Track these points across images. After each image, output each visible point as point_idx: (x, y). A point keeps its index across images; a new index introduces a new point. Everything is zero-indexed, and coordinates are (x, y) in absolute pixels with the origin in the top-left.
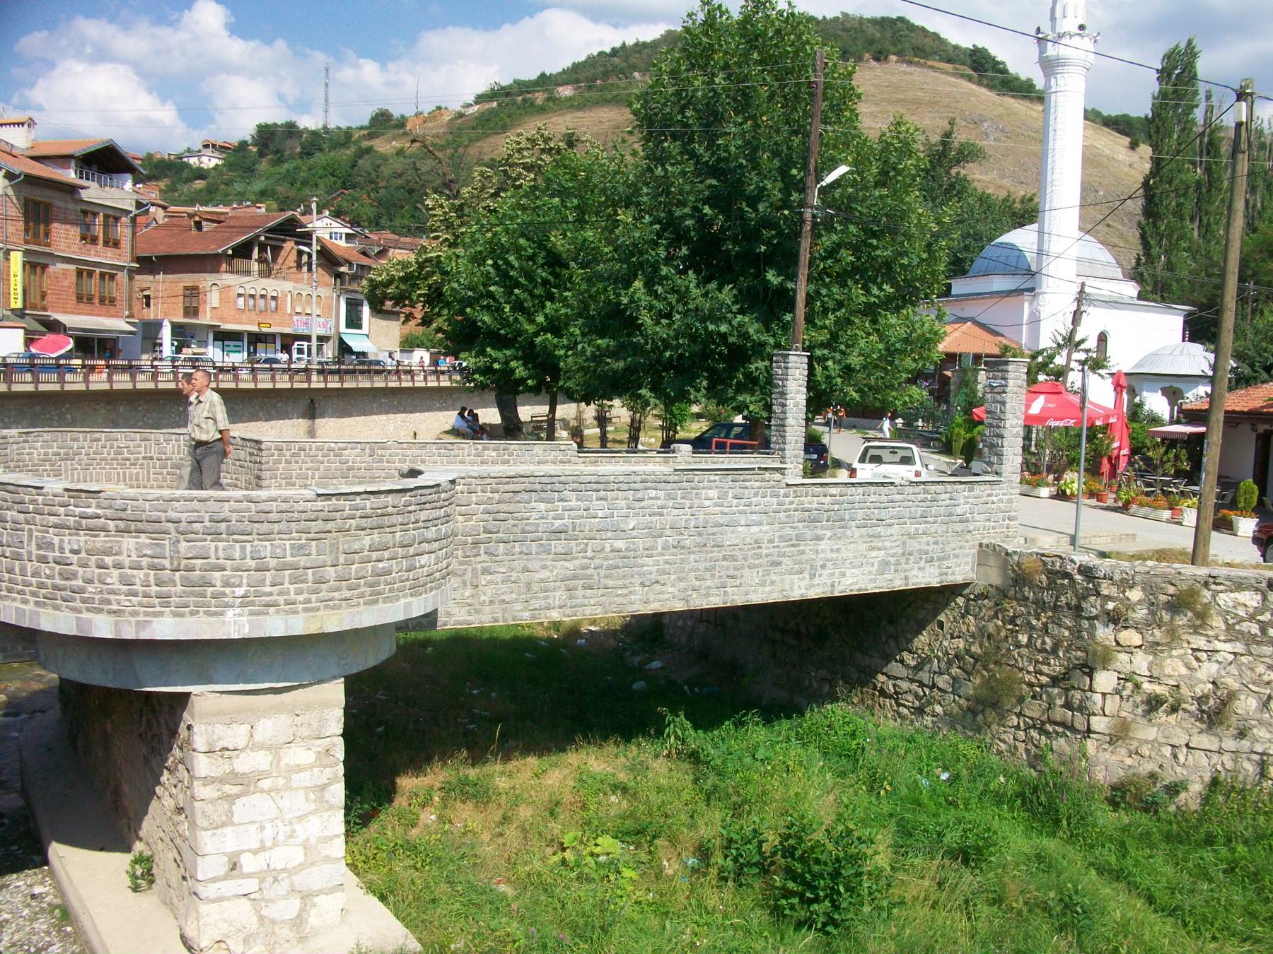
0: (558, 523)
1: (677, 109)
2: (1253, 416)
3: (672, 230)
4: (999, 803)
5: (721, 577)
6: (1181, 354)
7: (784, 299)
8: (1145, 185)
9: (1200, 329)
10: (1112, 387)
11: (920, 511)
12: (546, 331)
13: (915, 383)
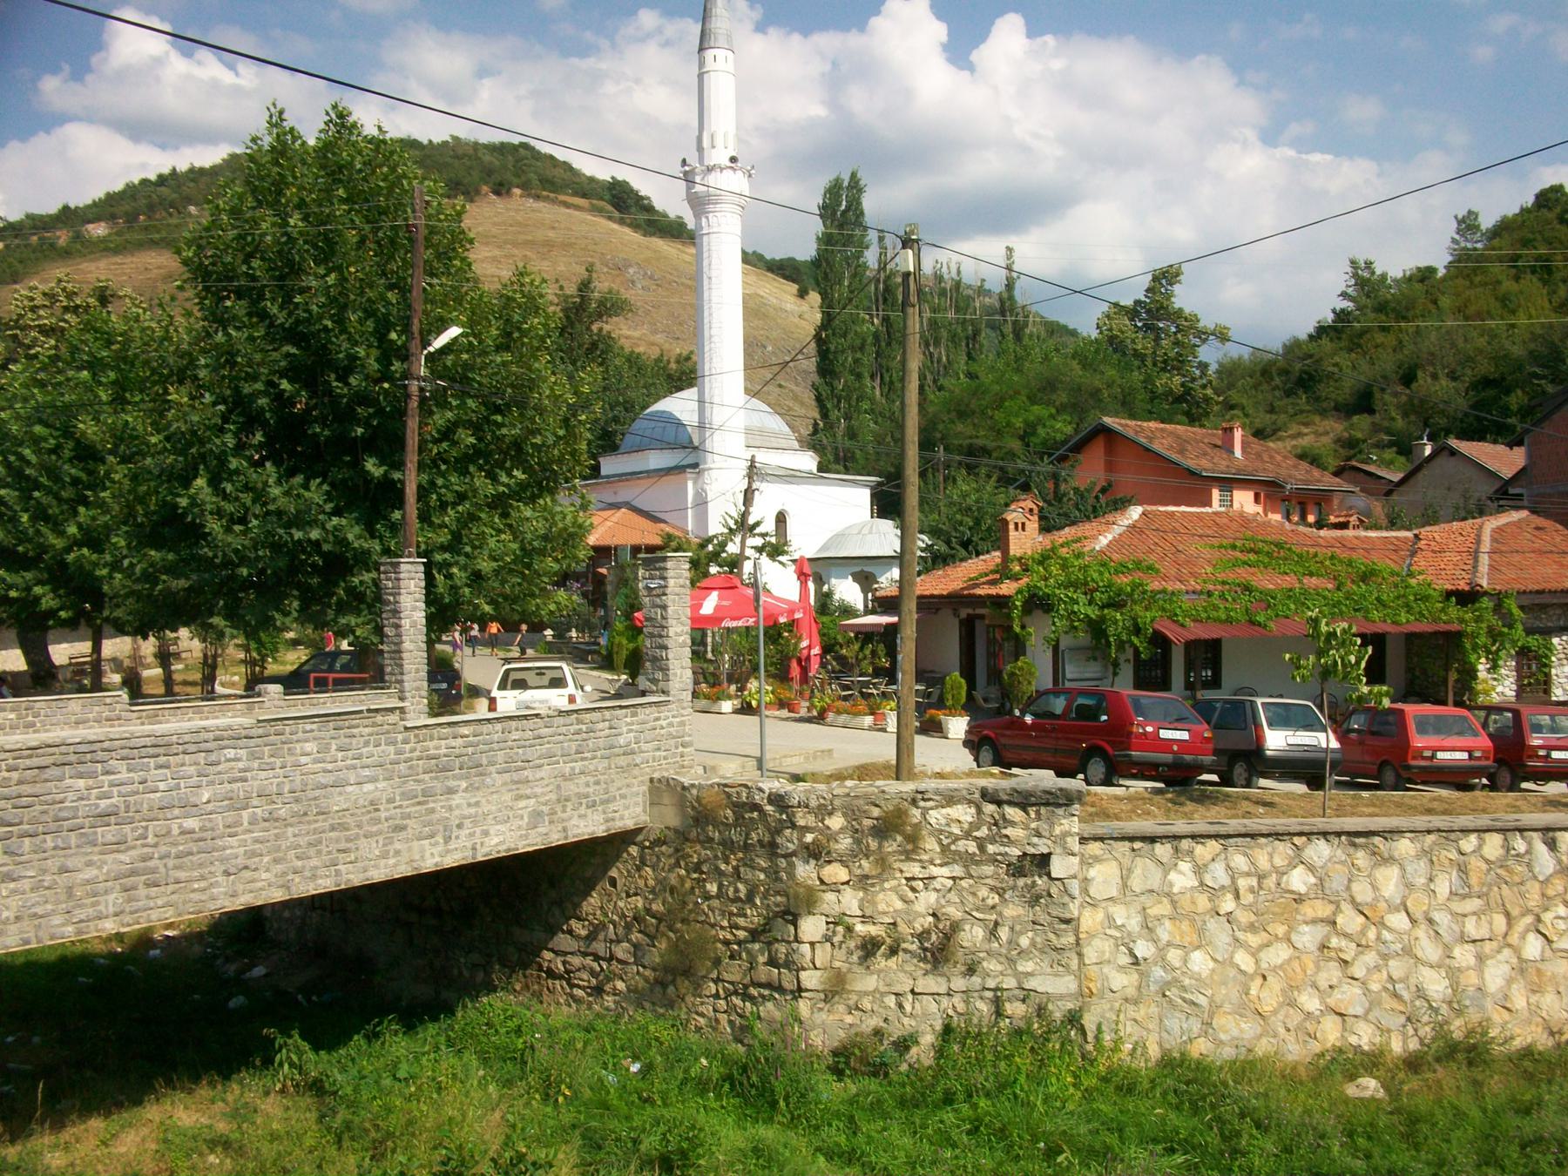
0: (103, 803)
1: (241, 257)
2: (954, 600)
3: (241, 410)
4: (703, 1092)
5: (329, 853)
7: (391, 494)
8: (818, 338)
9: (887, 505)
10: (795, 576)
11: (574, 746)
12: (80, 545)
13: (564, 585)
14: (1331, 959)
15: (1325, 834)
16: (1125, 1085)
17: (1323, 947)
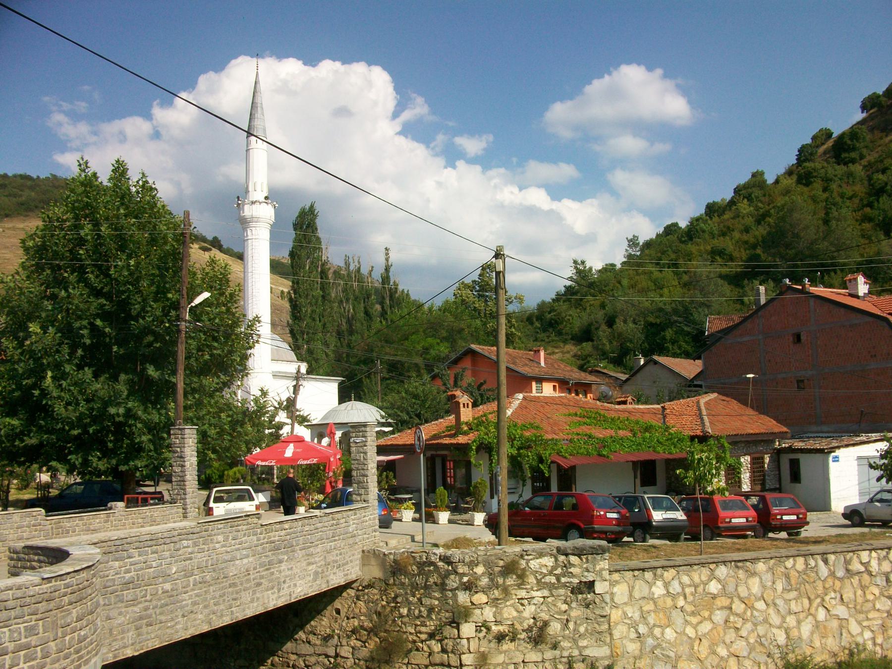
0: (128, 576)
7: (169, 389)
14: (730, 628)
15: (724, 562)
17: (726, 621)
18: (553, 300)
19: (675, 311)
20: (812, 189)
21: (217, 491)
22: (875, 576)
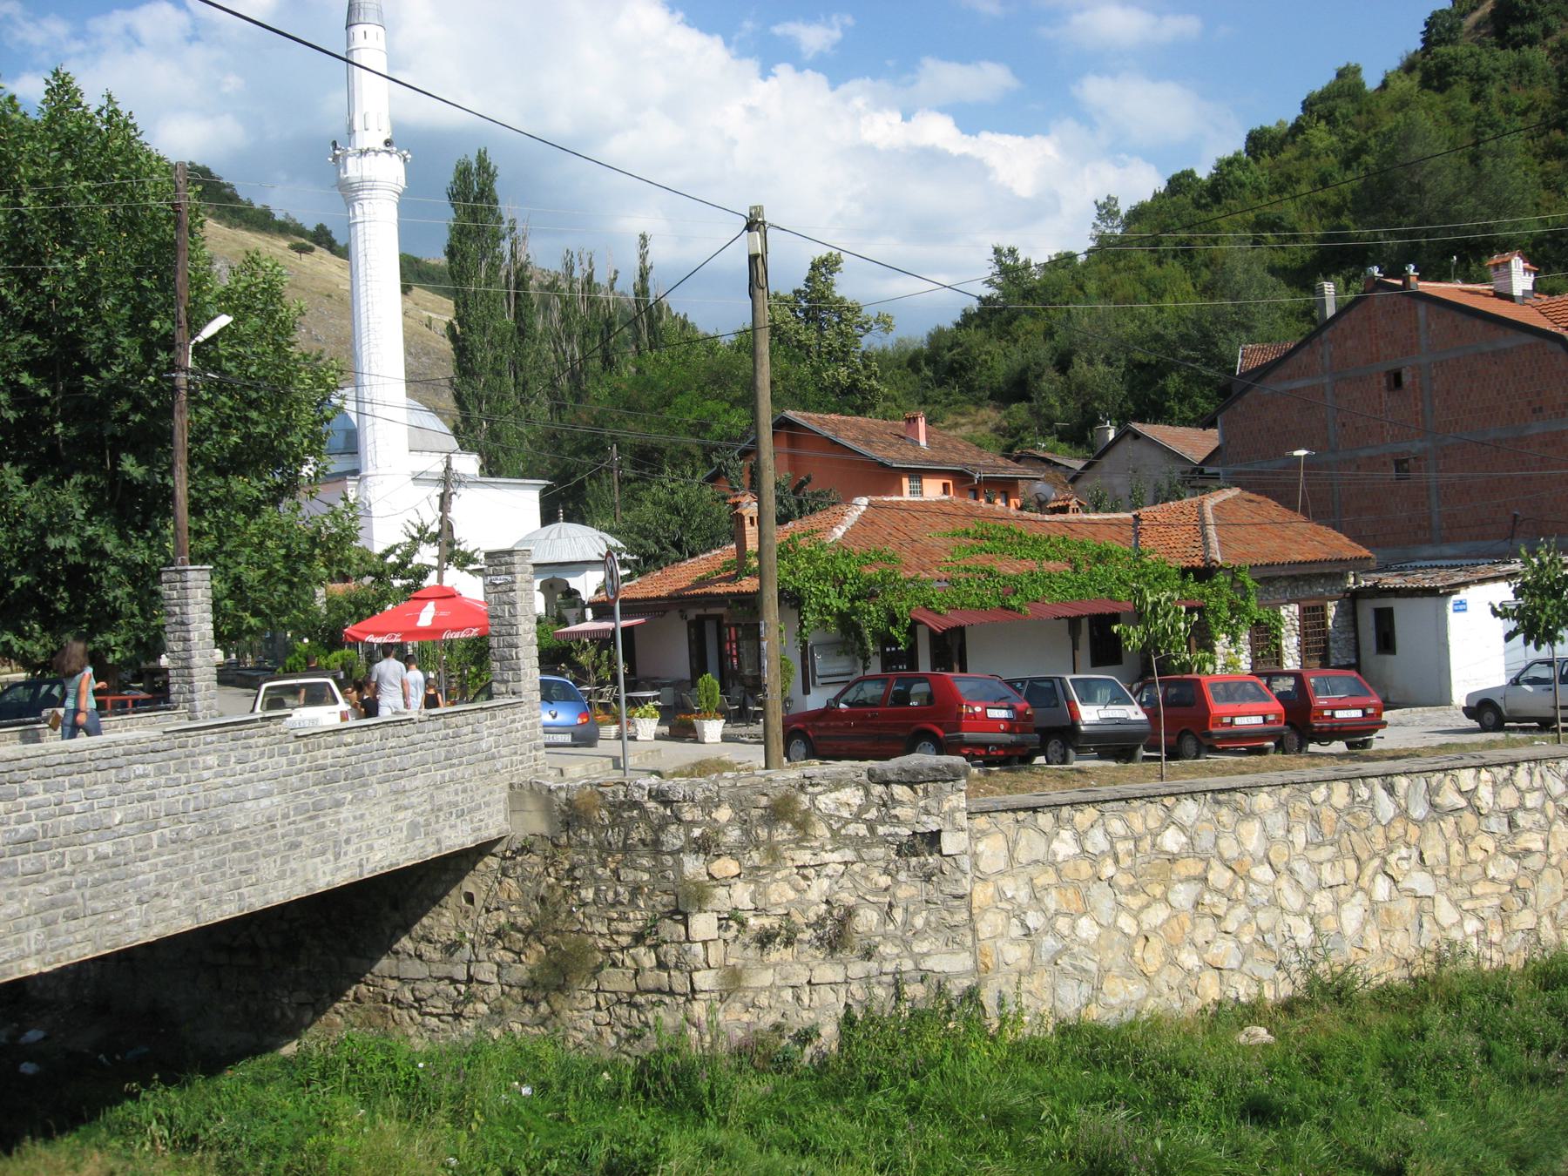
0: (23, 828)
2: (677, 602)
5: (233, 875)
6: (559, 537)
11: (443, 752)
14: (1205, 915)
16: (1033, 1054)
17: (1197, 904)
18: (958, 325)
19: (1185, 339)
20: (1451, 98)
21: (268, 689)
22: (1487, 816)
